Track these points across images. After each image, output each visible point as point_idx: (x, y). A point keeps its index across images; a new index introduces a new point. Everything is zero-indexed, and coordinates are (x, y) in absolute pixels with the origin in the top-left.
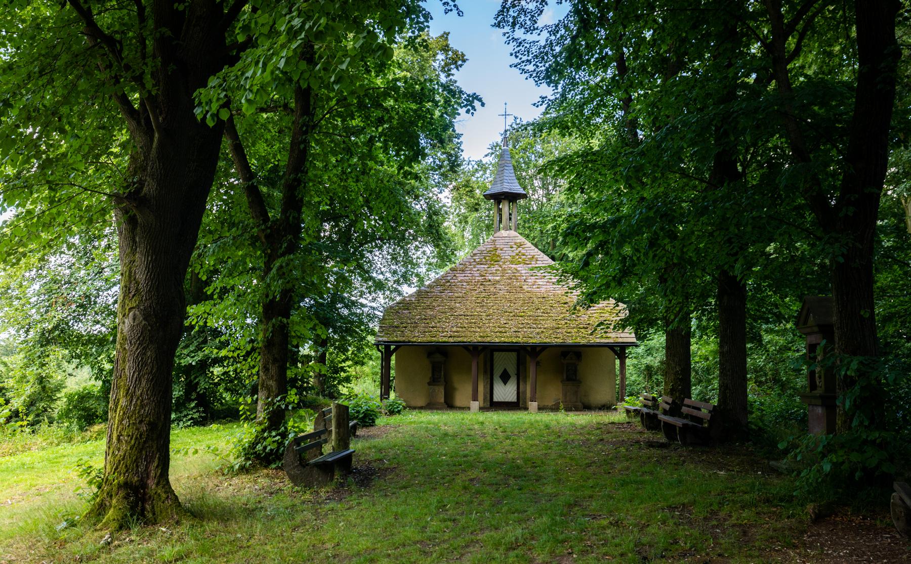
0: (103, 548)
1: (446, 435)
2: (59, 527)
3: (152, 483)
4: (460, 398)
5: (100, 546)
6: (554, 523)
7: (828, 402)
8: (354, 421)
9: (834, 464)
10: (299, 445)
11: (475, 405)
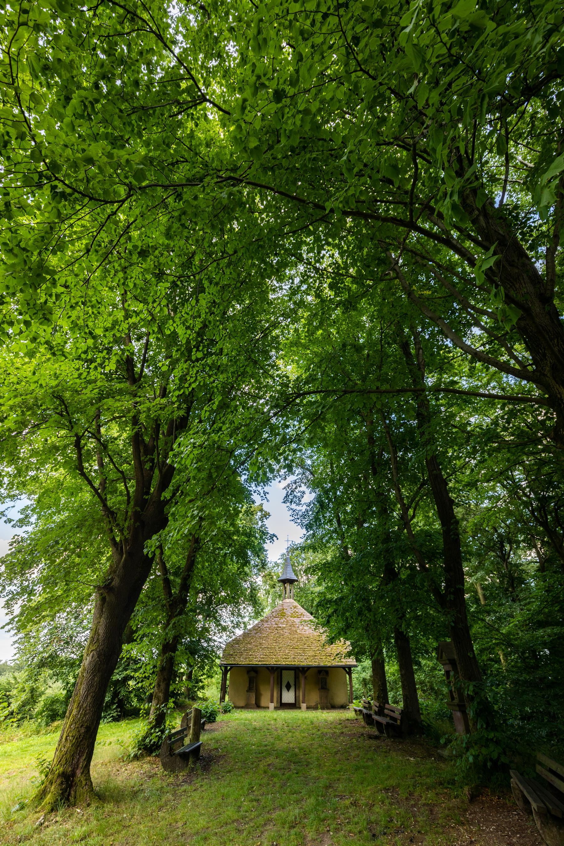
0: (37, 828)
1: (255, 729)
2: (14, 809)
3: (79, 772)
4: (264, 701)
5: (35, 827)
6: (318, 804)
7: (462, 708)
8: (204, 719)
9: (474, 756)
10: (170, 739)
11: (272, 706)
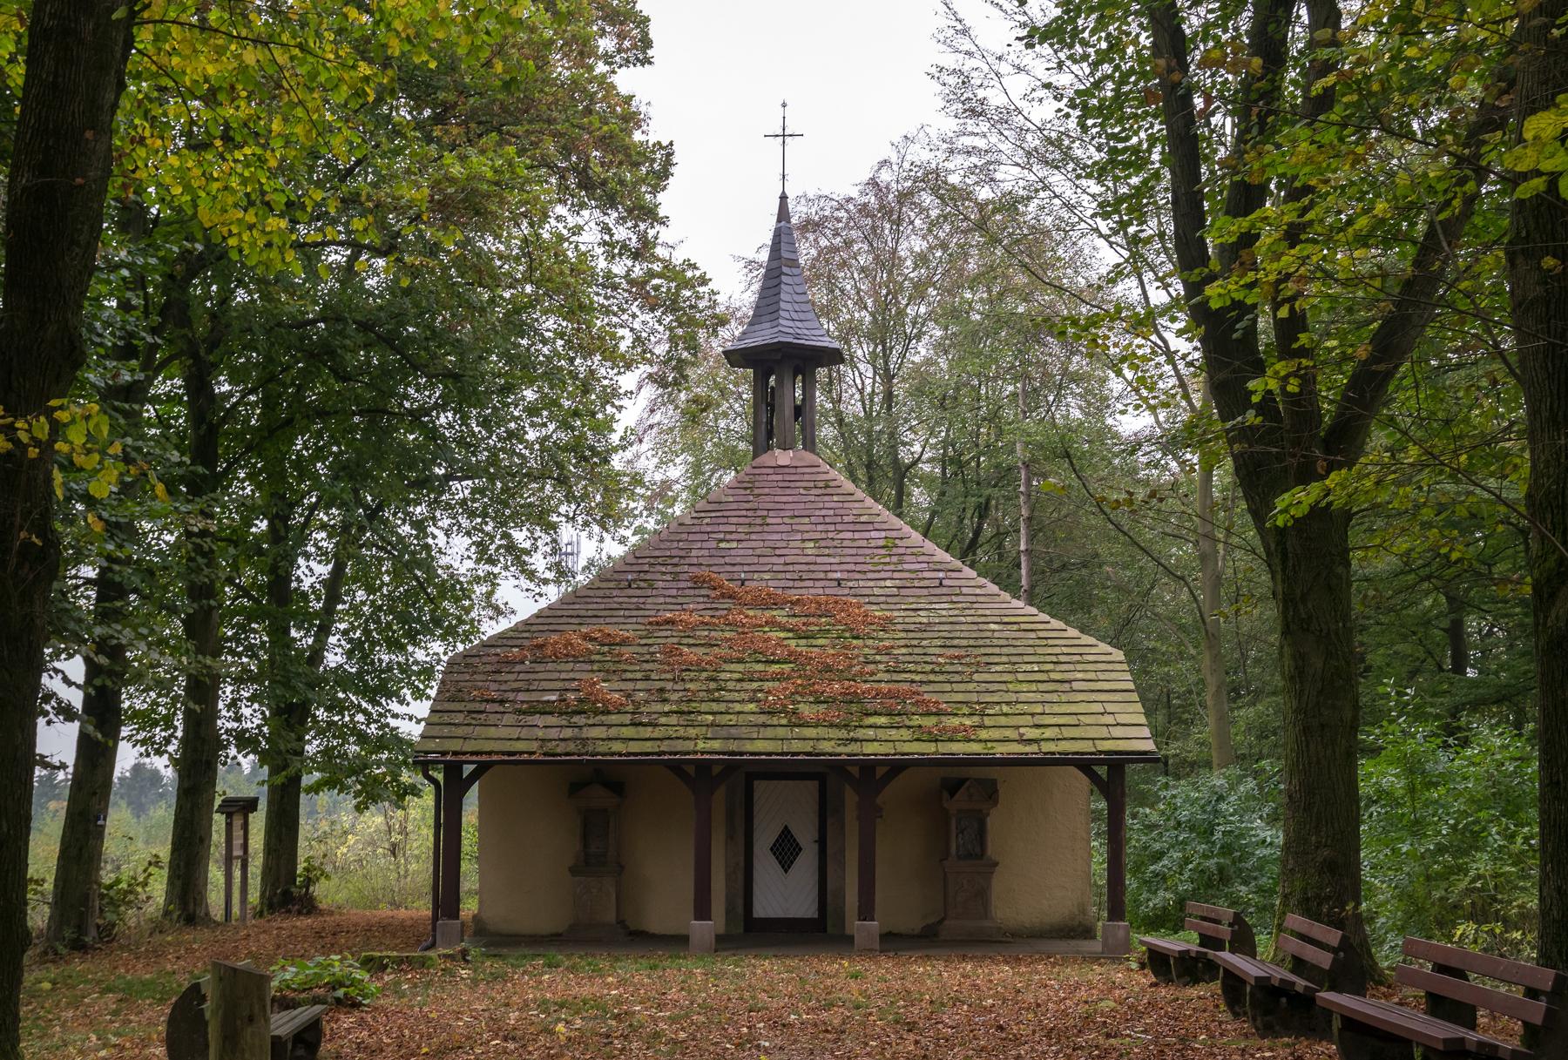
11: (703, 930)
